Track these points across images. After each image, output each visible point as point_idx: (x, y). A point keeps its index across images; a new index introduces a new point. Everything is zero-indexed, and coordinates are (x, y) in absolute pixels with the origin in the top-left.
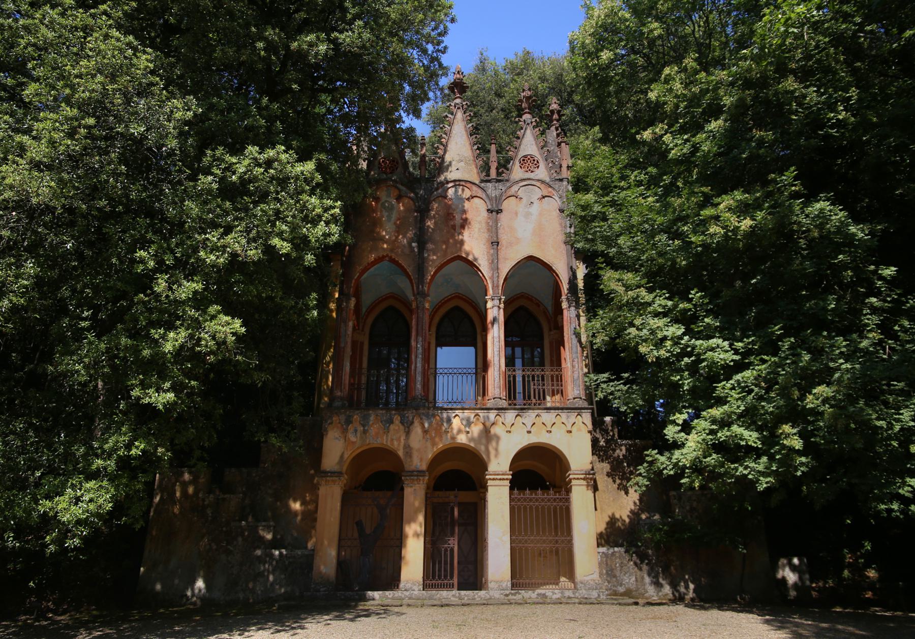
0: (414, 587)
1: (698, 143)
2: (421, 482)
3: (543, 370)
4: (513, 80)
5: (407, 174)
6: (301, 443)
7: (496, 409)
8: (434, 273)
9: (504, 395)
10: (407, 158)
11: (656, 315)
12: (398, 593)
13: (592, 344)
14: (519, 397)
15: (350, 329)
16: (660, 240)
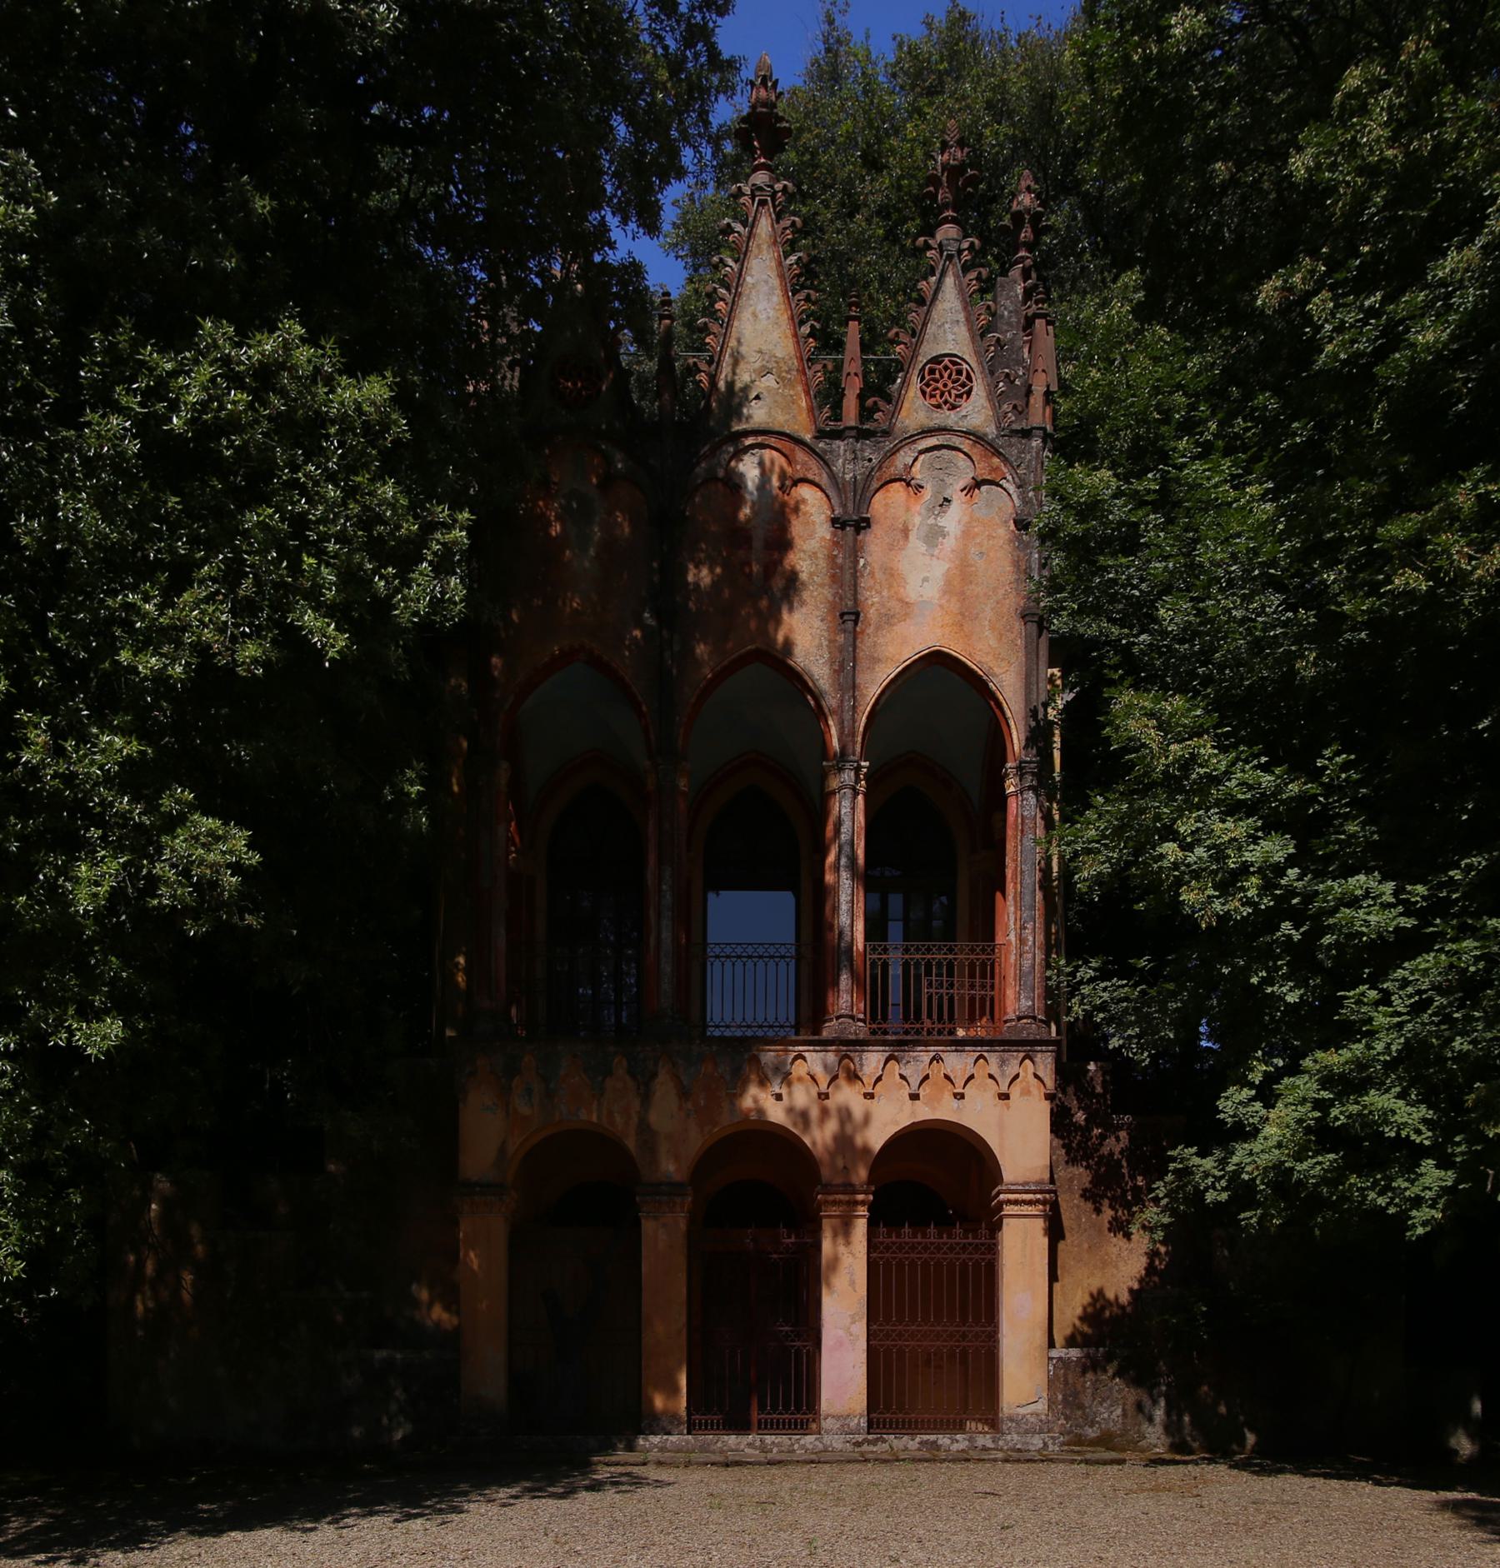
1: (1402, 321)
3: (951, 950)
4: (916, 112)
11: (1233, 809)
14: (895, 1014)
16: (1263, 607)
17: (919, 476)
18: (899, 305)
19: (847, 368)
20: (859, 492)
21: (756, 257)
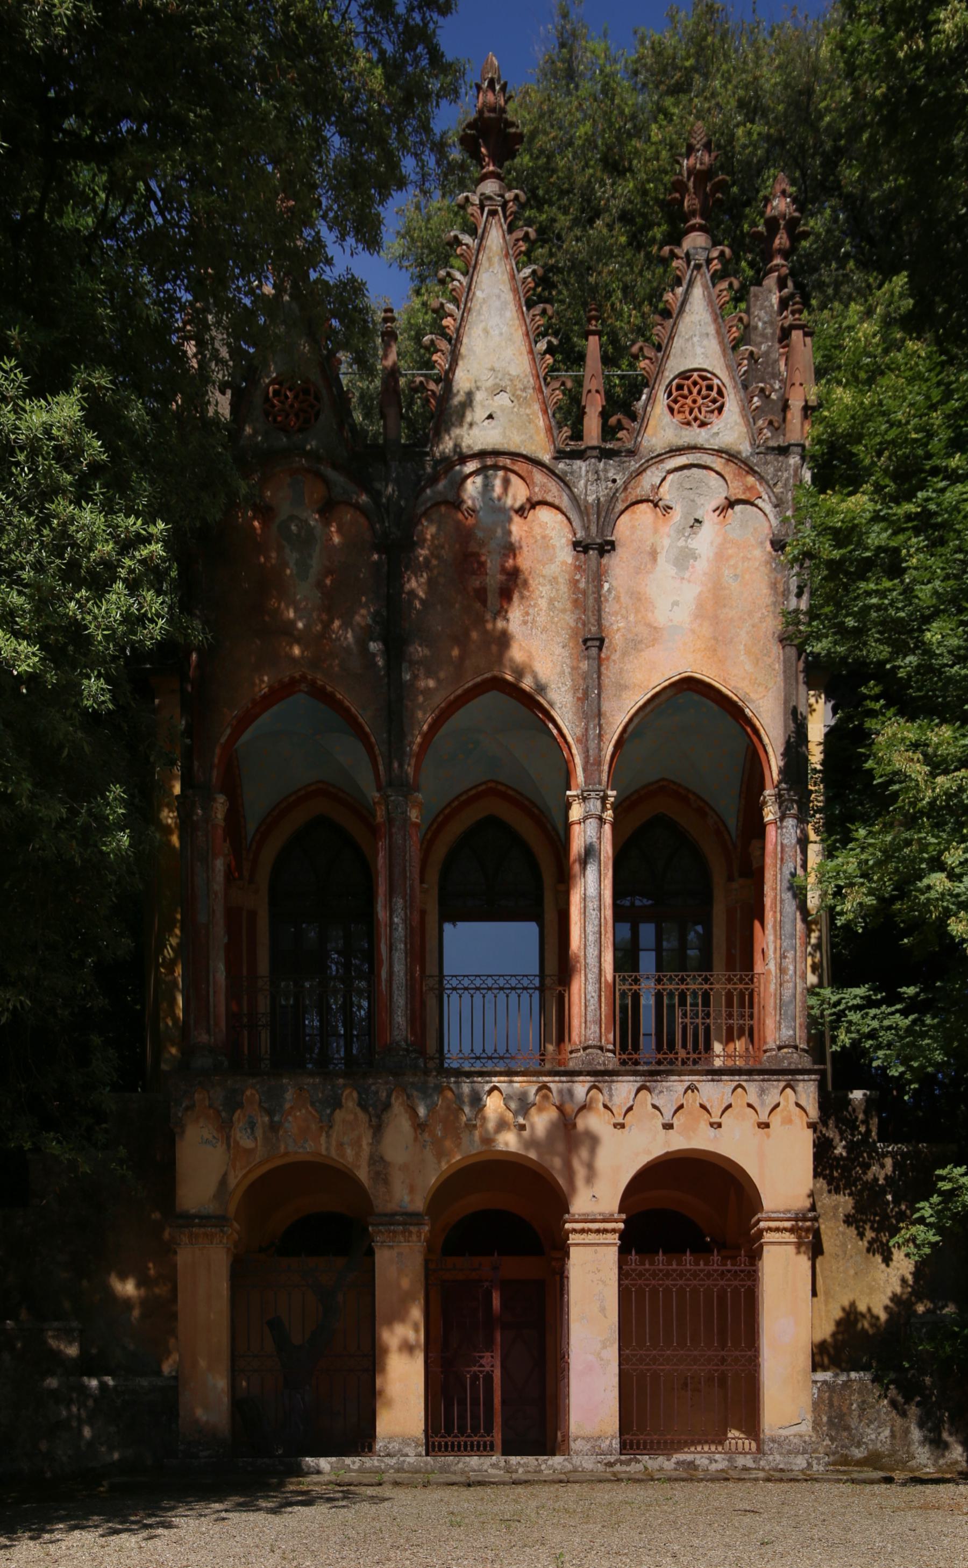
0: (407, 1450)
2: (414, 1238)
3: (706, 980)
5: (347, 434)
6: (122, 1151)
7: (589, 1074)
8: (431, 727)
9: (609, 1039)
10: (344, 380)
12: (370, 1462)
13: (832, 913)
14: (648, 1045)
15: (220, 878)
17: (667, 497)
18: (643, 316)
19: (587, 385)
20: (603, 514)
21: (487, 270)
